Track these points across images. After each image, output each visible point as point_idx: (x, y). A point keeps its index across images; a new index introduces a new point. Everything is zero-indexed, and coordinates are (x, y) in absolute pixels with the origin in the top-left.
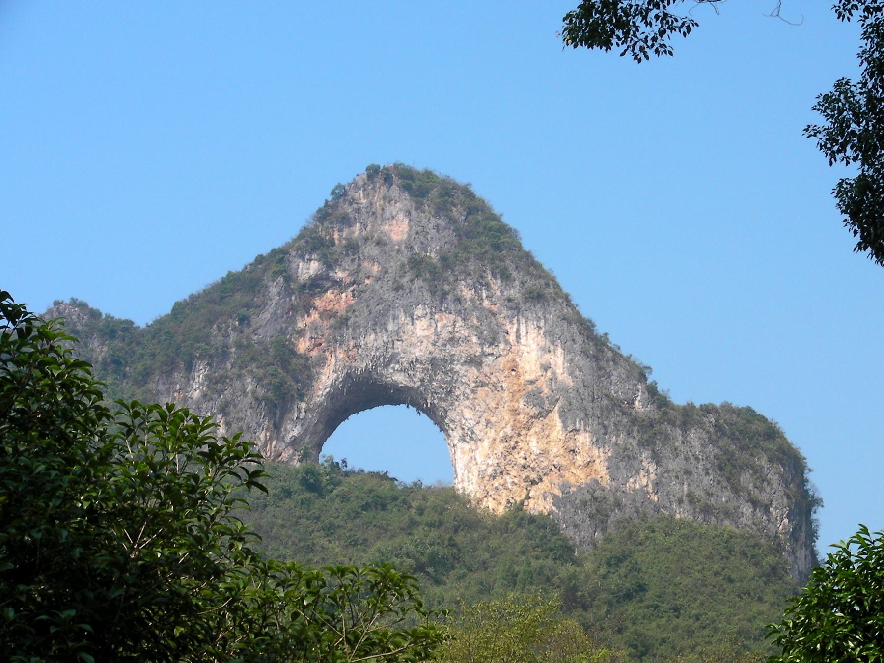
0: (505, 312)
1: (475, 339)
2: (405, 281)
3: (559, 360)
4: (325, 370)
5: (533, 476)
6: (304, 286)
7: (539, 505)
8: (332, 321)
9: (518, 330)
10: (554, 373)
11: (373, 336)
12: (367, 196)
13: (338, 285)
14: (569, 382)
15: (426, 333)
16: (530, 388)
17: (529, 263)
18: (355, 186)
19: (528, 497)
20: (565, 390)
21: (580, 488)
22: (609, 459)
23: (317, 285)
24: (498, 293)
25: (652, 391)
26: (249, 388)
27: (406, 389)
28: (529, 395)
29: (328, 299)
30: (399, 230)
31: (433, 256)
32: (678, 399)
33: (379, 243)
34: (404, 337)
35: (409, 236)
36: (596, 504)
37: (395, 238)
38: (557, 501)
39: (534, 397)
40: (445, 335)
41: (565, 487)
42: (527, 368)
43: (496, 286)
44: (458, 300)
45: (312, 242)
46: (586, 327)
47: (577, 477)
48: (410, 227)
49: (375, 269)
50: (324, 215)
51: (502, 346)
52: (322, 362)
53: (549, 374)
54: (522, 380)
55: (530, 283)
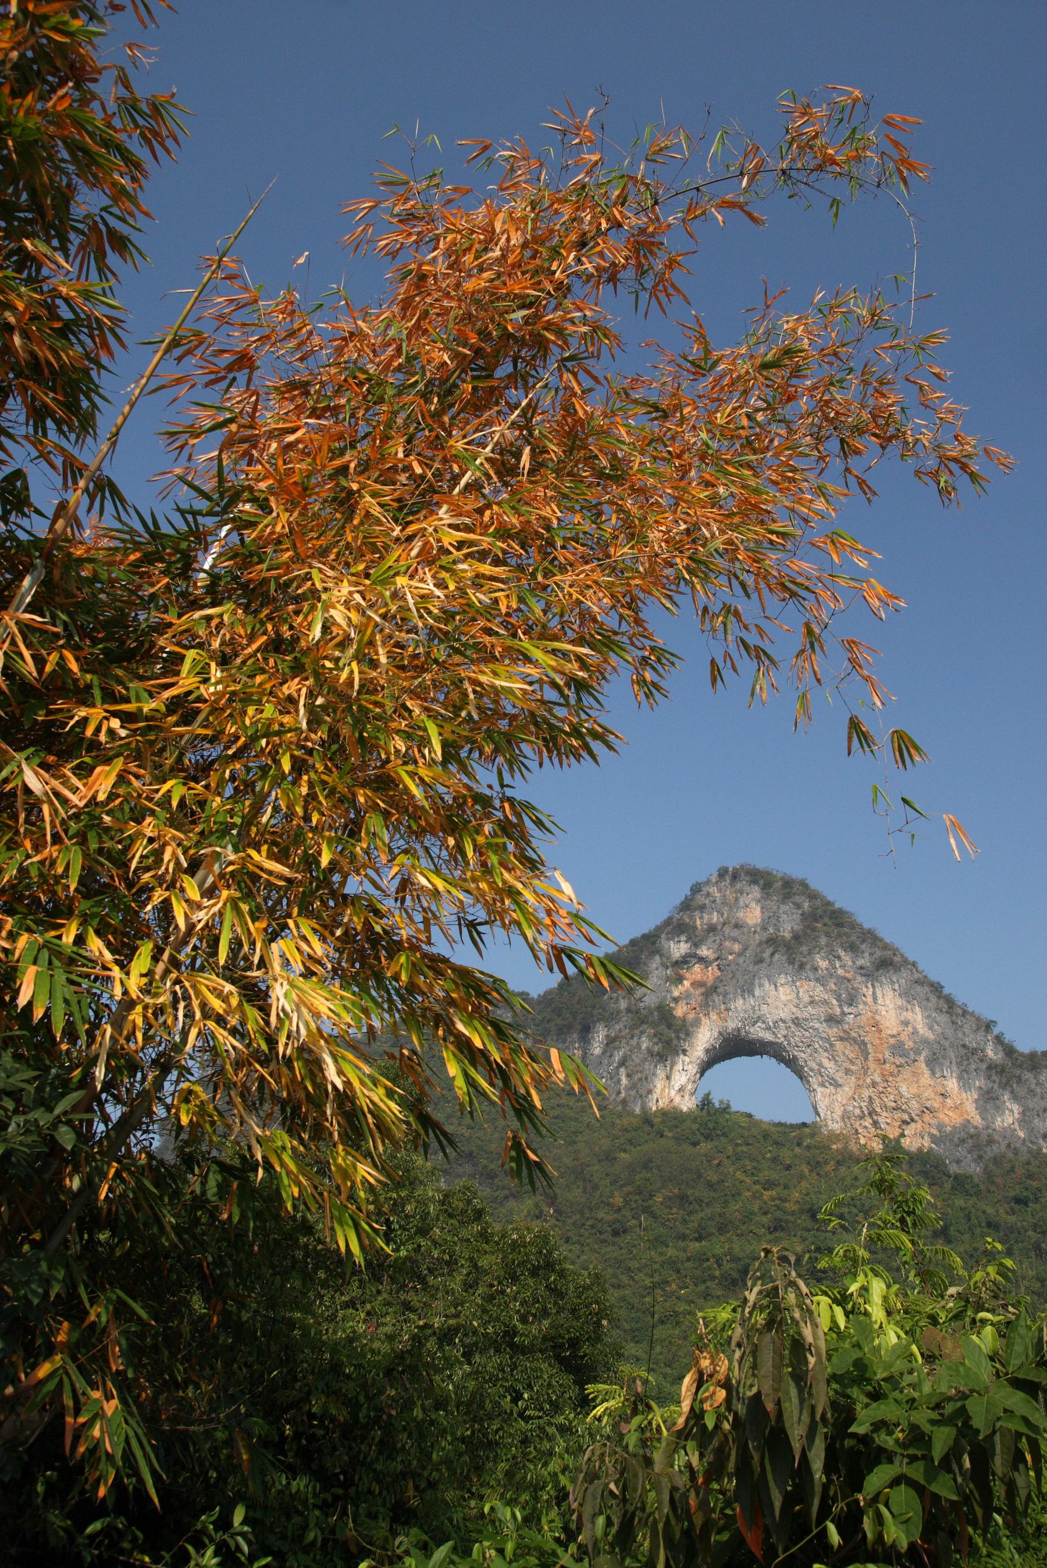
0: (859, 978)
1: (835, 1002)
2: (960, 1012)
3: (917, 1017)
4: (701, 1030)
5: (906, 1117)
6: (677, 962)
7: (911, 1142)
8: (703, 990)
9: (874, 993)
10: (914, 1028)
11: (741, 1001)
12: (720, 891)
13: (701, 960)
14: (931, 1036)
15: (789, 997)
16: (892, 1041)
17: (870, 937)
18: (708, 882)
19: (903, 1135)
20: (926, 1042)
21: (954, 1127)
22: (976, 1101)
23: (684, 961)
24: (850, 963)
25: (999, 1039)
26: (644, 1046)
27: (771, 1043)
28: (893, 1047)
29: (697, 971)
30: (753, 914)
31: (787, 935)
32: (1024, 1046)
33: (737, 926)
34: (770, 1001)
35: (763, 920)
36: (974, 1140)
37: (750, 922)
38: (933, 1139)
39: (898, 1048)
40: (807, 999)
41: (940, 1127)
42: (888, 1024)
43: (847, 958)
44: (815, 969)
45: (676, 927)
46: (936, 988)
47: (950, 1119)
48: (762, 913)
49: (737, 947)
50: (686, 906)
51: (861, 1007)
52: (697, 1023)
53: (910, 1029)
54: (883, 1035)
55: (878, 953)
